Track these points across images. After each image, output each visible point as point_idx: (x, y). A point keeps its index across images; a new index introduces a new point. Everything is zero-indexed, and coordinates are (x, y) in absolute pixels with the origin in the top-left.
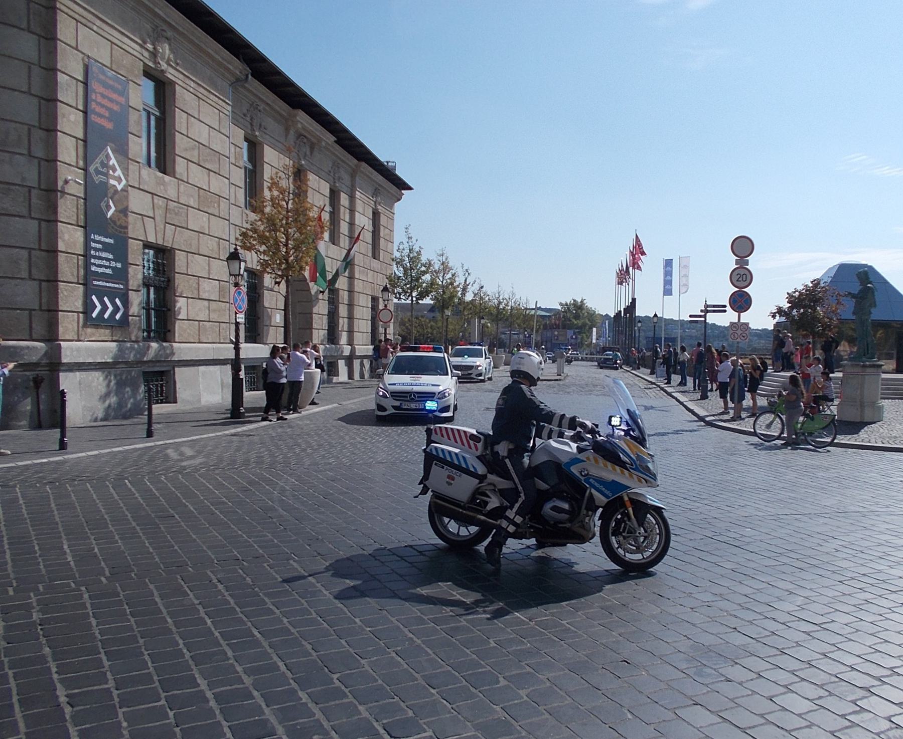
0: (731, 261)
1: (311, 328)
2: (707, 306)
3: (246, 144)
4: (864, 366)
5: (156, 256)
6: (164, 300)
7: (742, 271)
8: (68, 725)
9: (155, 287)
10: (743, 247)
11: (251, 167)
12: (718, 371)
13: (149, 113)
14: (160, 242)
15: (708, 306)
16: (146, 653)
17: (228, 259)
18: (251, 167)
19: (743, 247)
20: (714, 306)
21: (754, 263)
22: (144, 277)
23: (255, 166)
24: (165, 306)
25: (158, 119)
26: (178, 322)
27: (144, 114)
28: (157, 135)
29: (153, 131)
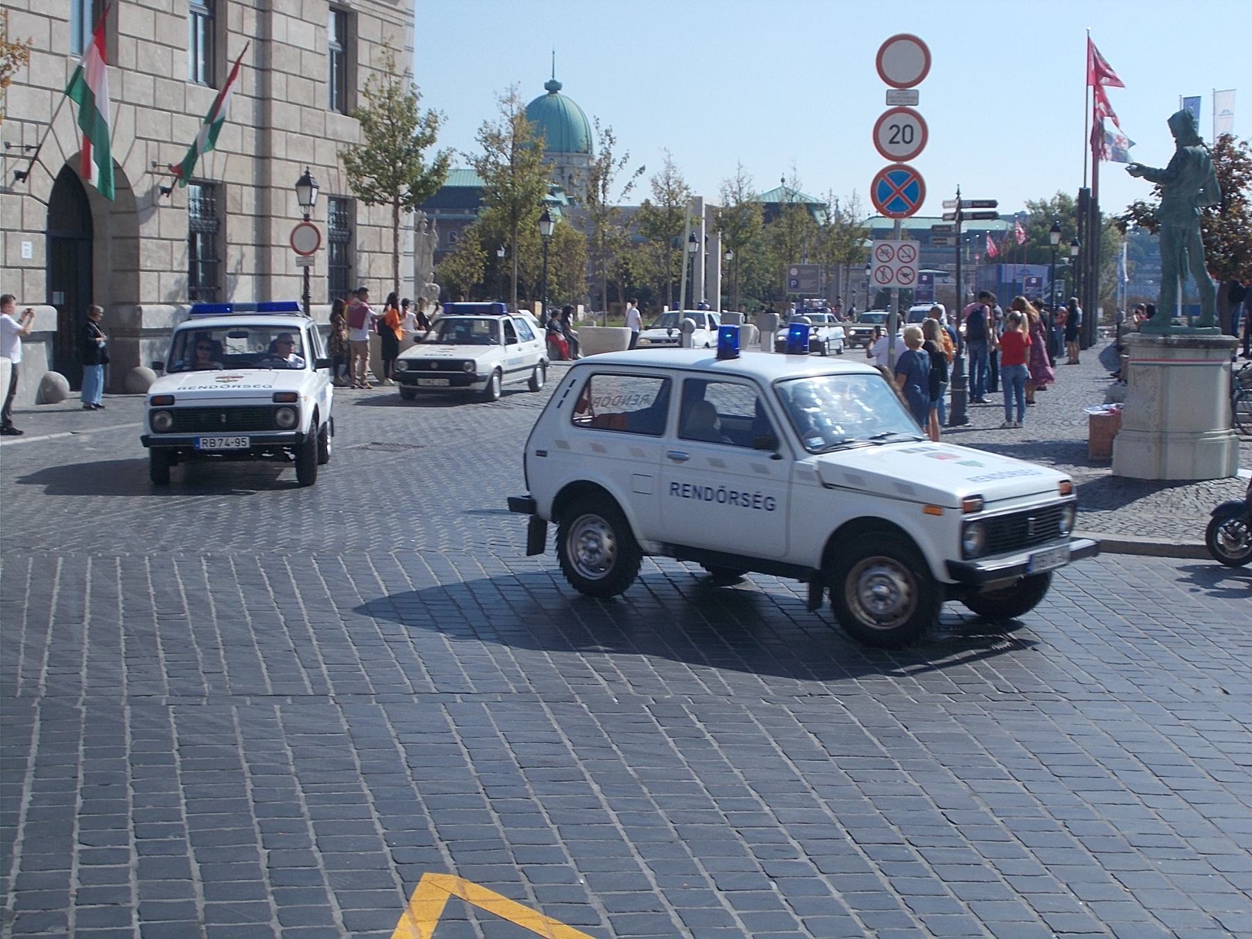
0: (874, 98)
1: (137, 270)
2: (961, 205)
3: (332, 16)
4: (1167, 345)
5: (203, 193)
6: (214, 250)
7: (901, 119)
8: (25, 788)
9: (202, 233)
10: (904, 61)
11: (339, 49)
12: (1050, 378)
13: (195, 15)
14: (208, 176)
15: (961, 205)
16: (256, 820)
17: (298, 184)
18: (339, 49)
19: (904, 61)
20: (974, 204)
21: (930, 99)
22: (191, 222)
23: (345, 47)
24: (215, 256)
25: (206, 18)
26: (45, 265)
27: (190, 17)
28: (206, 37)
29: (200, 32)
